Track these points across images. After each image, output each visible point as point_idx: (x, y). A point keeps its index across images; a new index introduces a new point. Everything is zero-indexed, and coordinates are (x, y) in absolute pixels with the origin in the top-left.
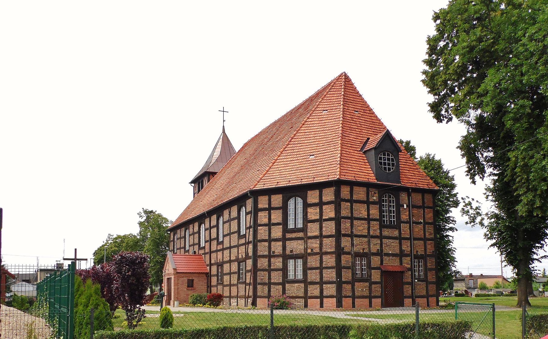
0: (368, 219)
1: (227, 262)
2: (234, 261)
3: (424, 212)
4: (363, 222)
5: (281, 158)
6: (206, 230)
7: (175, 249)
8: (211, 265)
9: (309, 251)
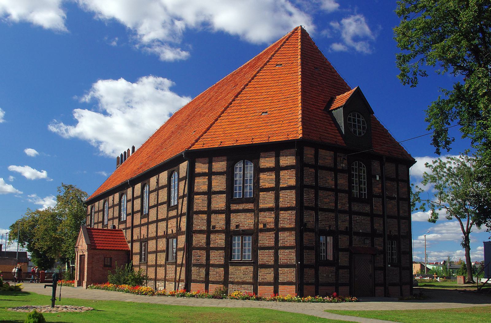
0: (336, 190)
1: (152, 239)
2: (161, 237)
3: (398, 185)
4: (330, 193)
6: (128, 201)
8: (132, 241)
9: (261, 226)
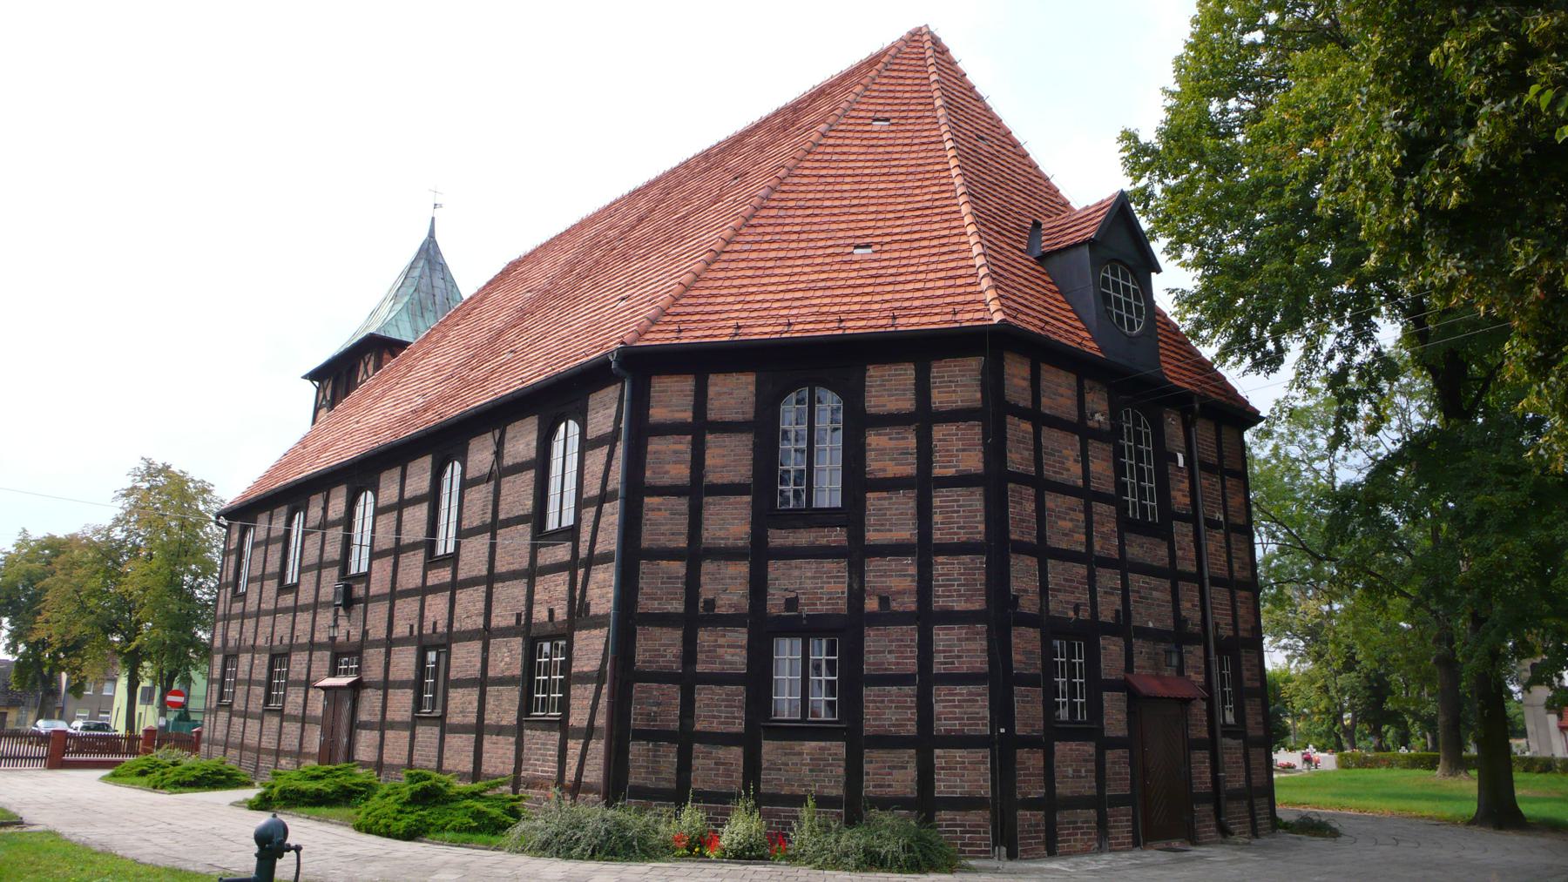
2: (403, 641)
5: (737, 247)
7: (243, 581)
9: (871, 604)
